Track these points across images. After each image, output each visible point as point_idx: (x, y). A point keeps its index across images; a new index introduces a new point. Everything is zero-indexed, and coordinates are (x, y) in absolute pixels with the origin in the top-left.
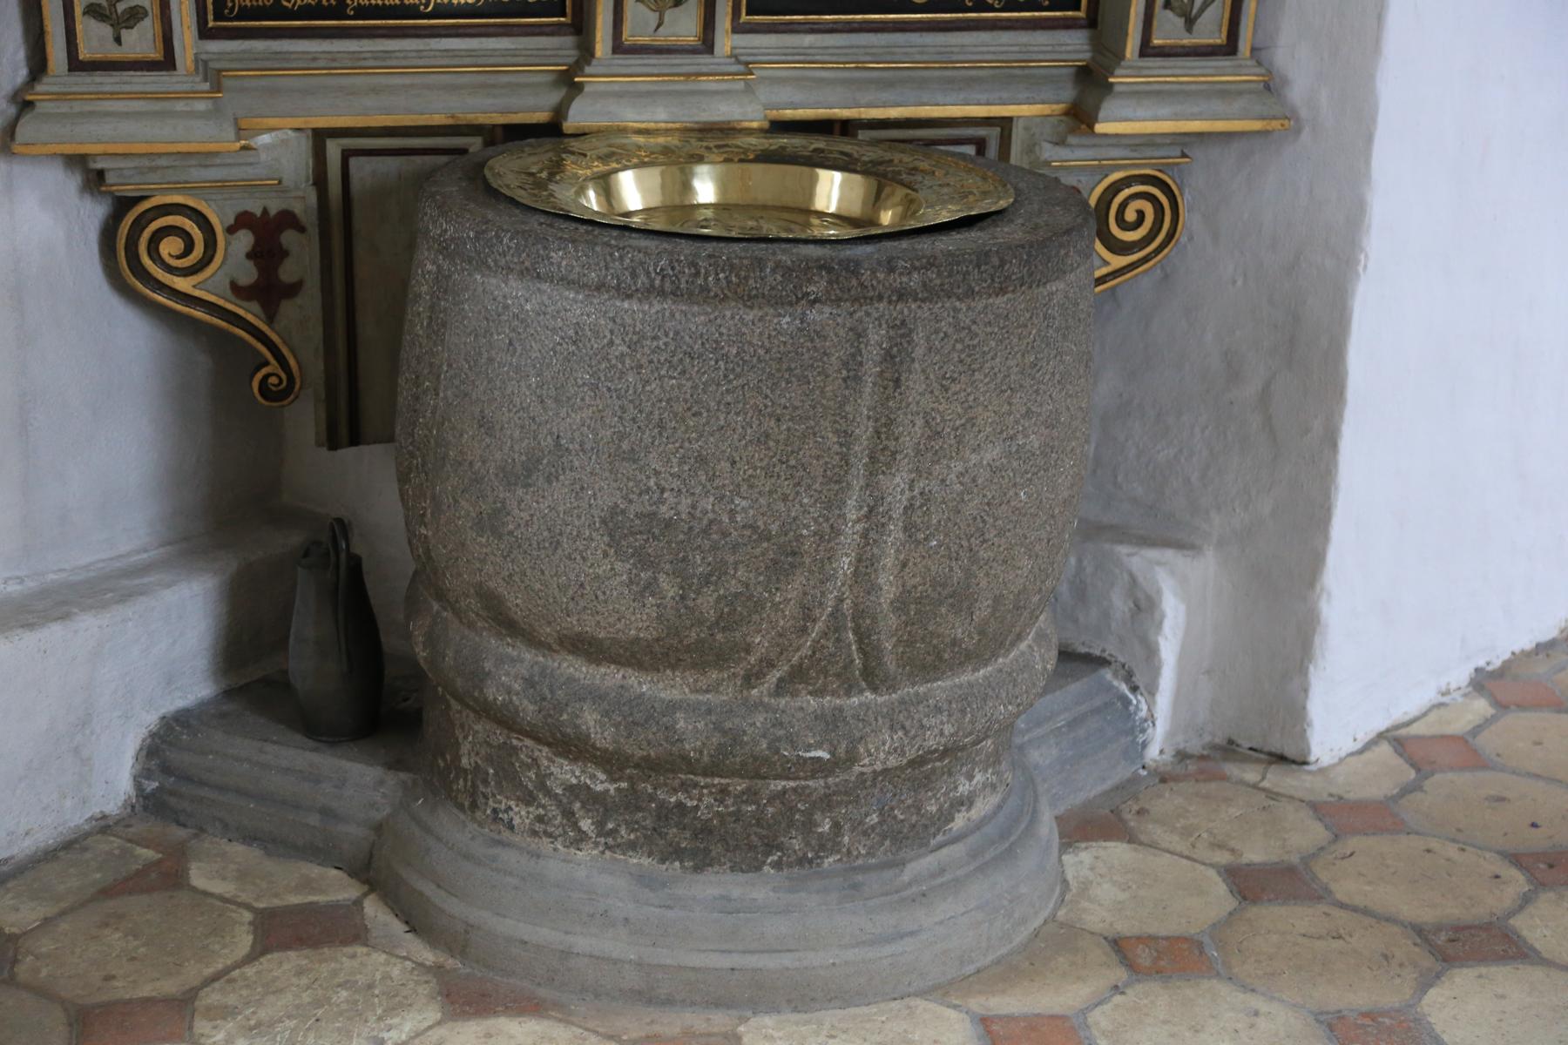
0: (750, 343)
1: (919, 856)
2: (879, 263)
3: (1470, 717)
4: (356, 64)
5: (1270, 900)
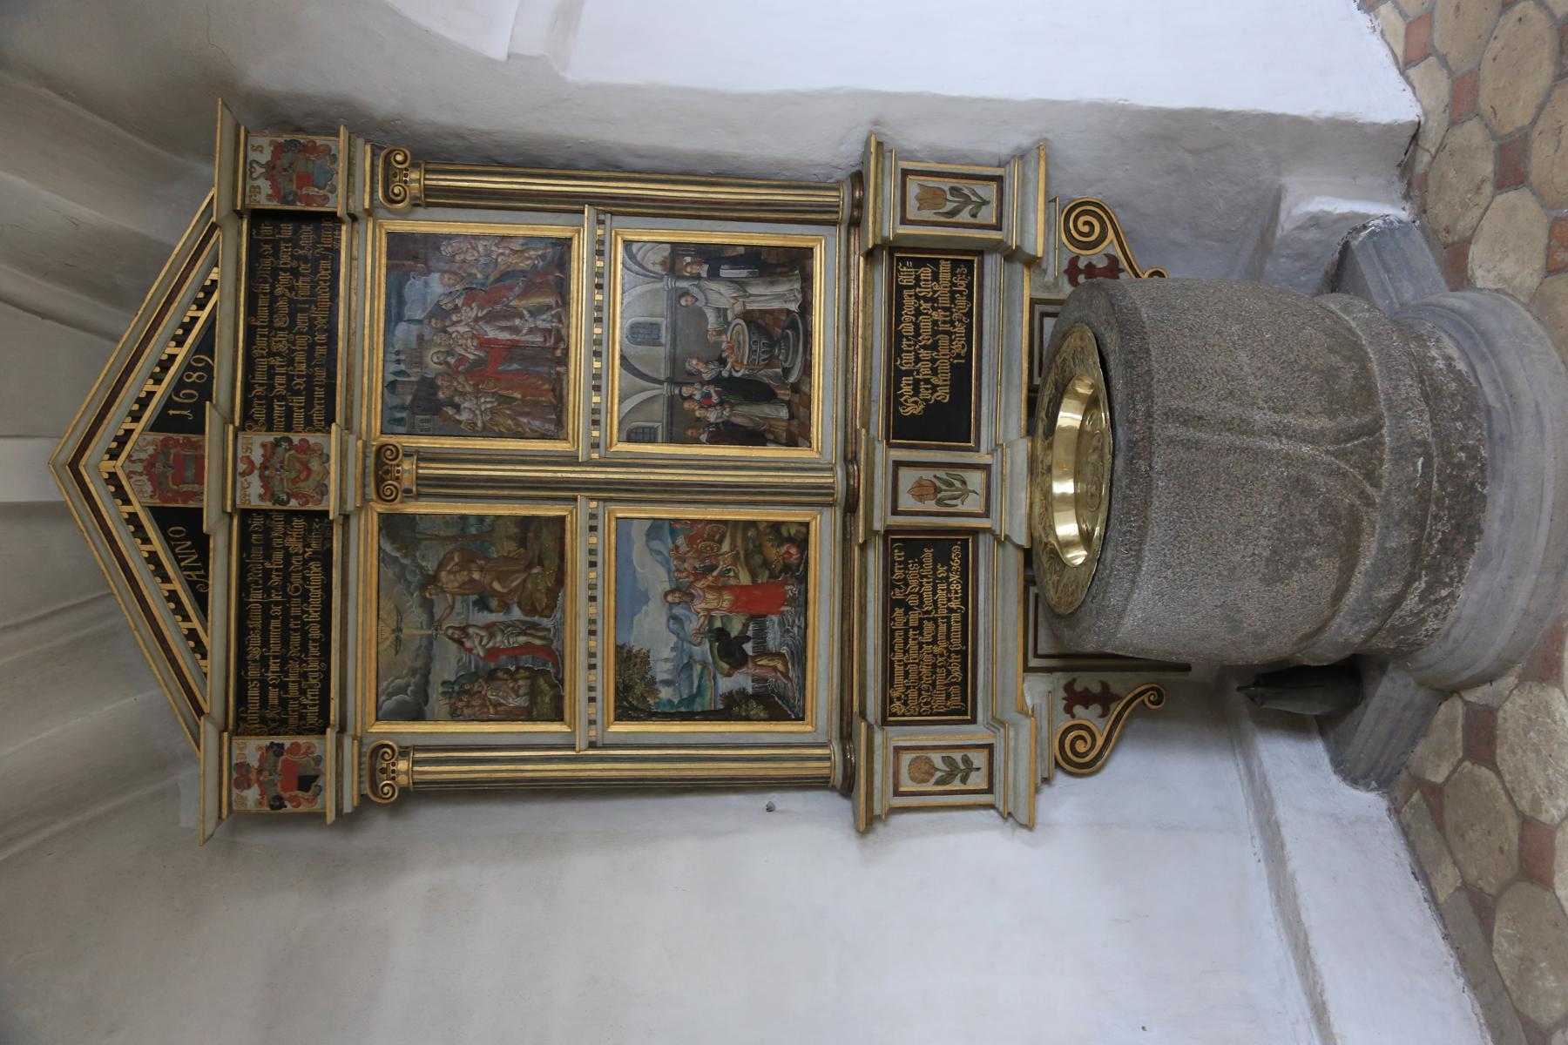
0: (1172, 504)
1: (1484, 395)
3: (1393, 17)
4: (991, 648)
5: (1525, 167)
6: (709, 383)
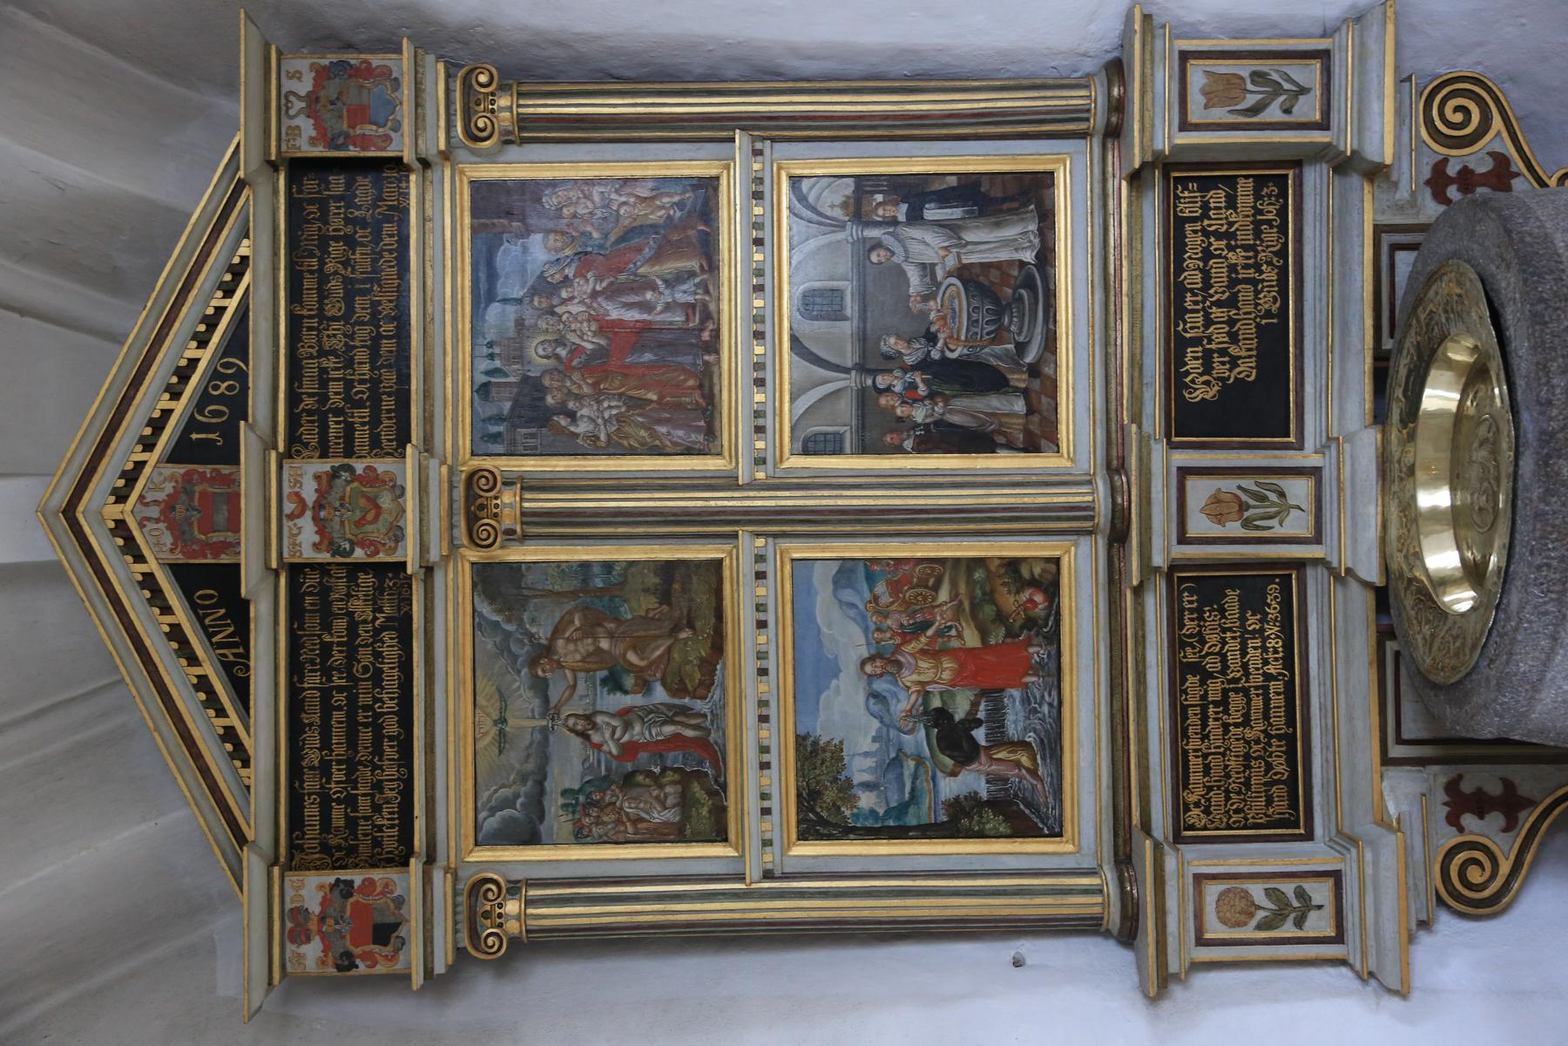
2: (1542, 413)
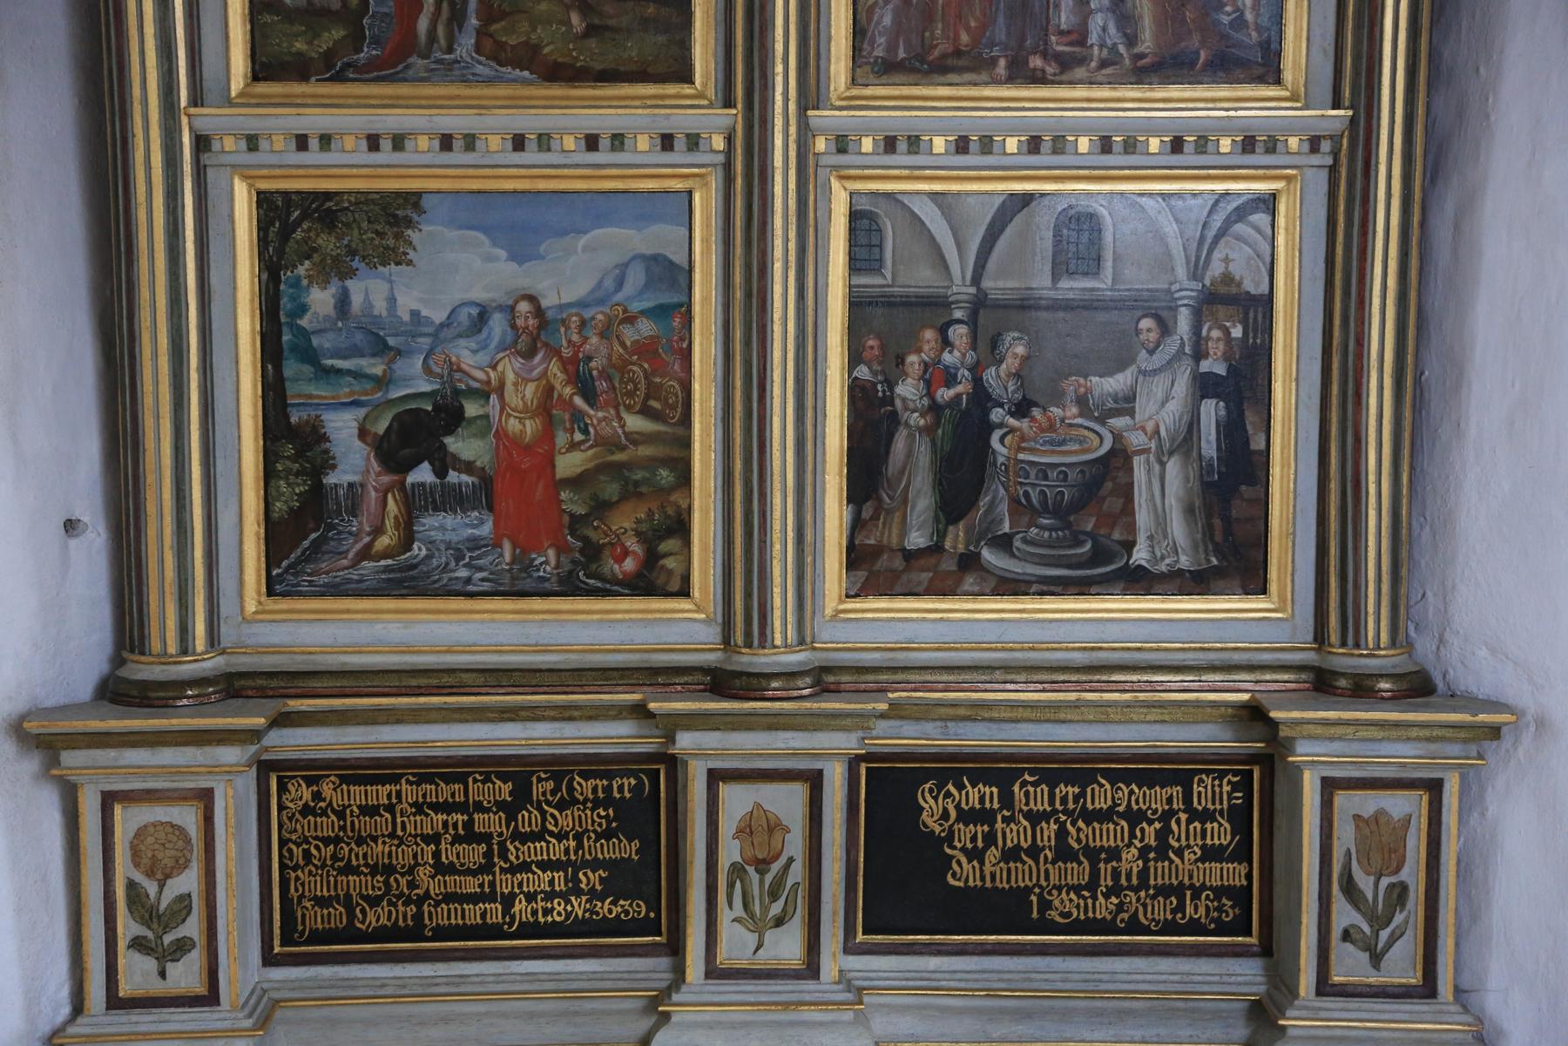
4: (426, 992)
6: (977, 381)
